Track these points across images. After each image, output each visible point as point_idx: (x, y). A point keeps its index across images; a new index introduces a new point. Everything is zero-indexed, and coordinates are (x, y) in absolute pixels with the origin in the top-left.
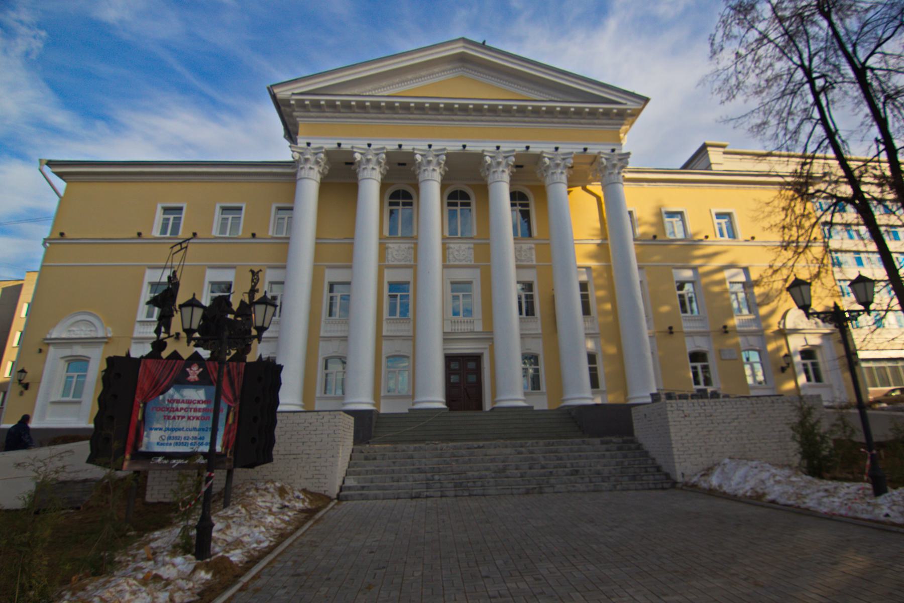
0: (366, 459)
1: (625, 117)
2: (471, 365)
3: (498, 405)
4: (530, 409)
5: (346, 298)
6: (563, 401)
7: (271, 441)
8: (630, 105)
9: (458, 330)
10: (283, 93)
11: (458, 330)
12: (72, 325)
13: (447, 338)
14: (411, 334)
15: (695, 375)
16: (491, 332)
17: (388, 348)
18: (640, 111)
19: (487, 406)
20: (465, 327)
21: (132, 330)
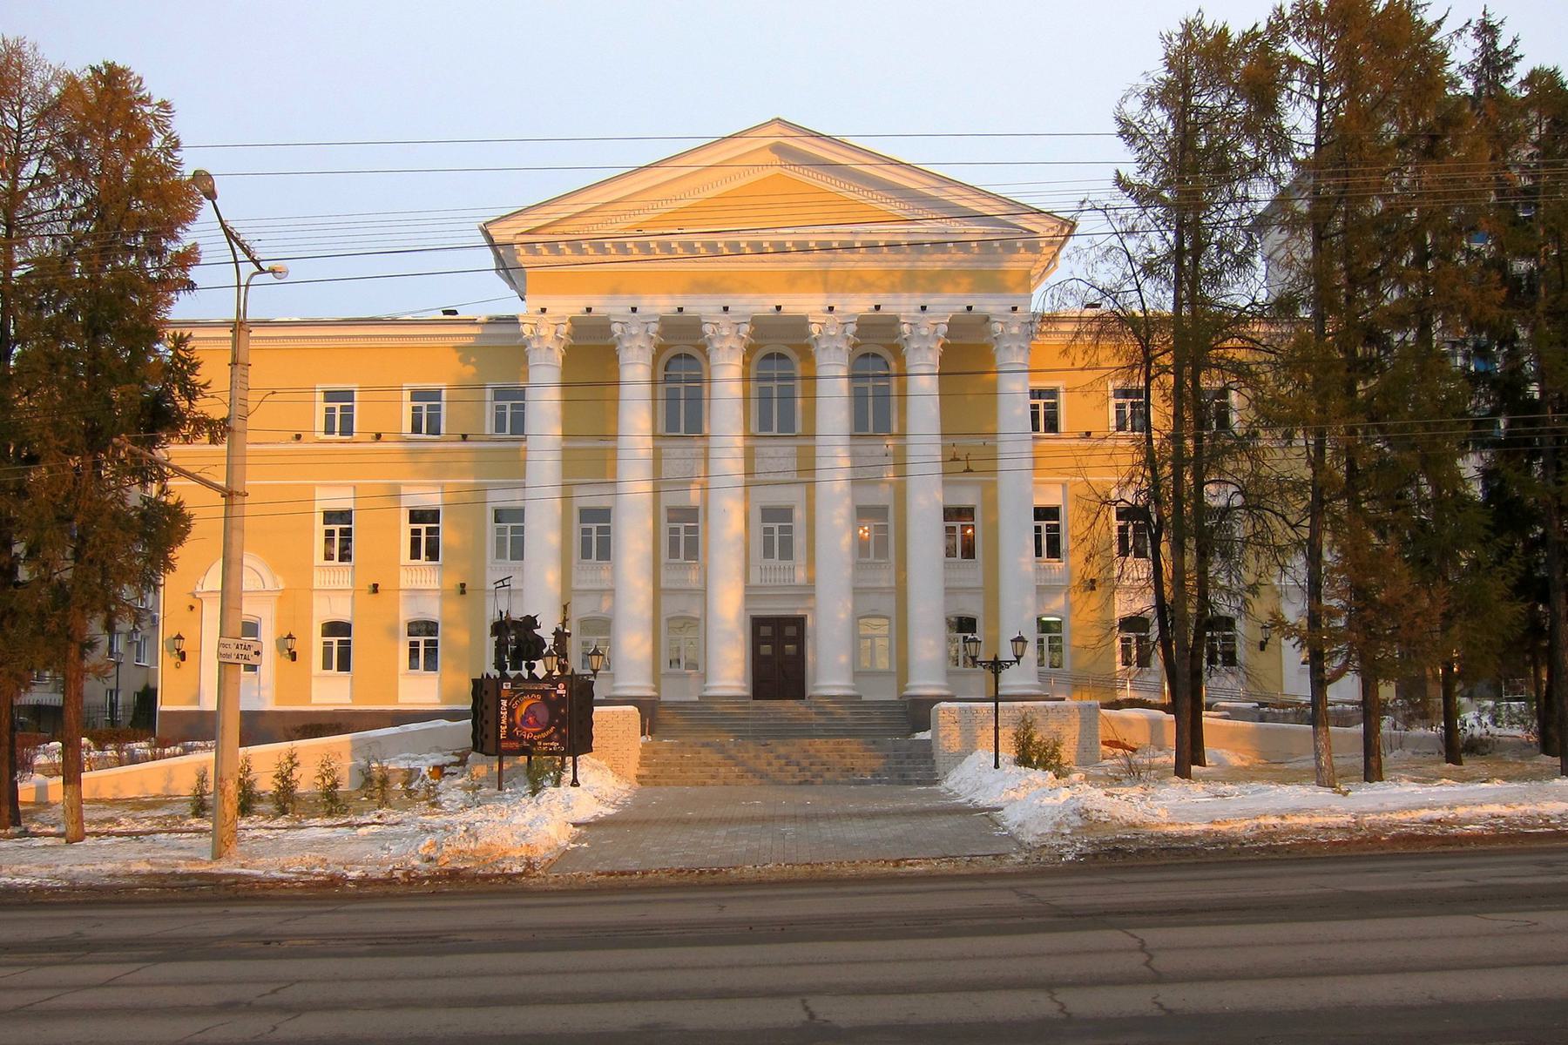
2: (791, 631)
5: (605, 532)
6: (615, 689)
9: (785, 580)
10: (501, 234)
11: (785, 580)
13: (750, 593)
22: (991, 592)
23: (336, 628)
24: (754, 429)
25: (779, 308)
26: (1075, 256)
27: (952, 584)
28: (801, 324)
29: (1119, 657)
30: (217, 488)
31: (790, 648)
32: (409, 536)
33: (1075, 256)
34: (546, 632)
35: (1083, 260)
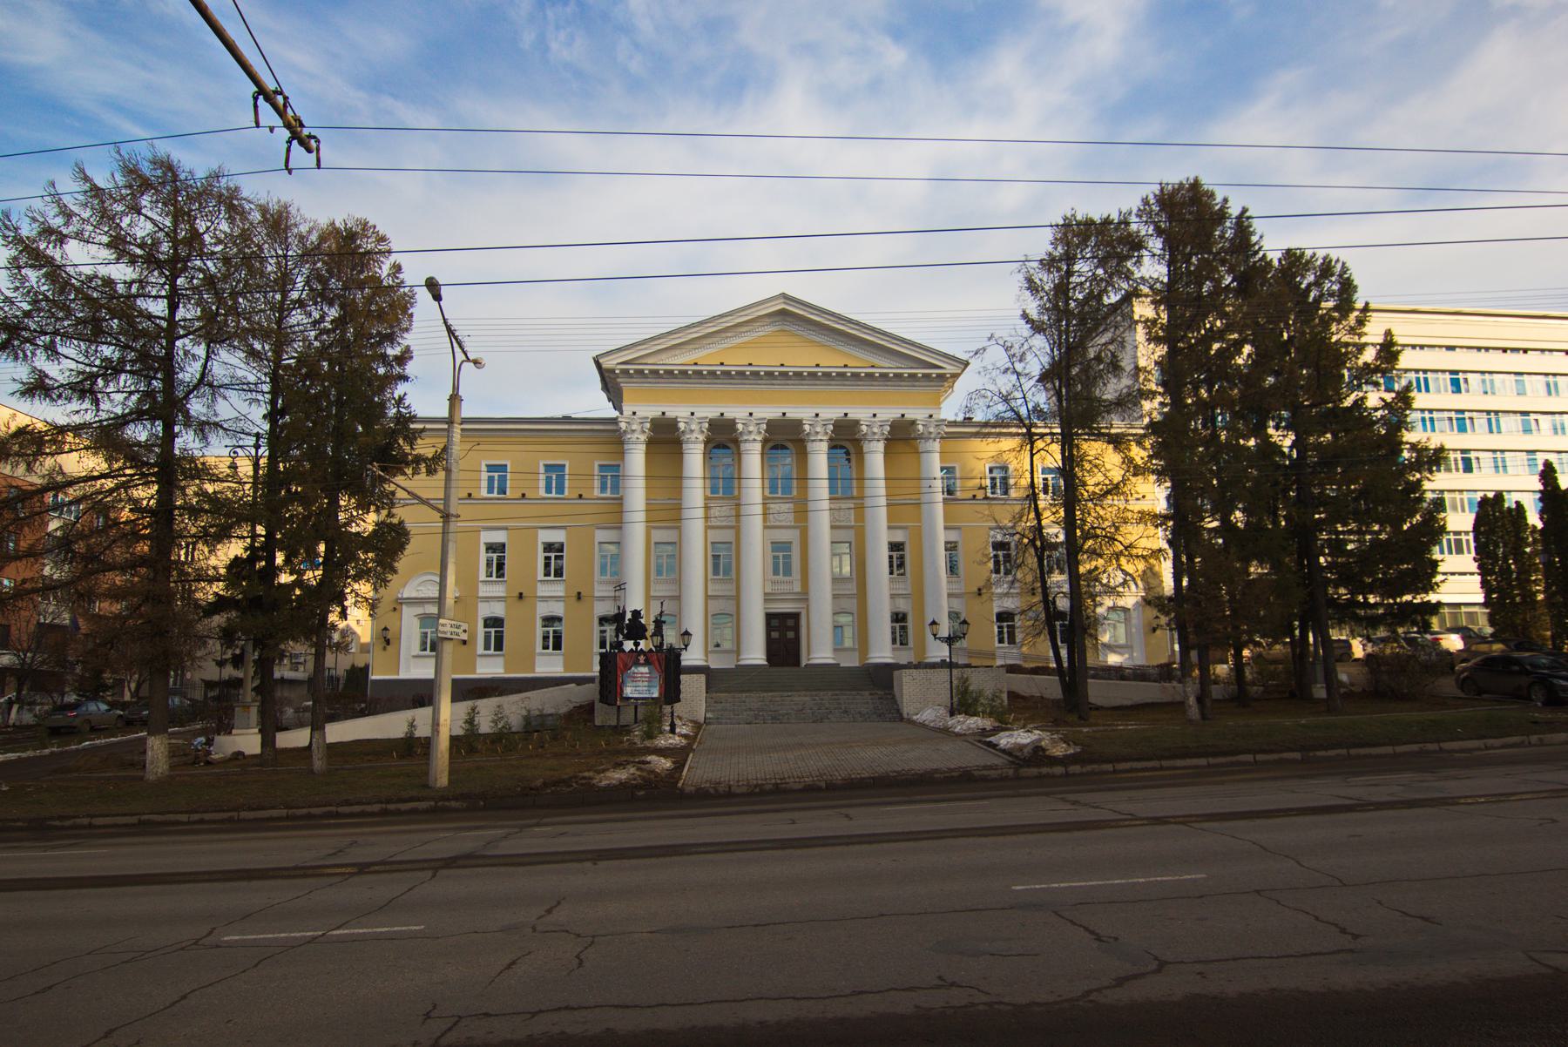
0: (716, 702)
1: (944, 381)
2: (790, 623)
3: (811, 662)
4: (837, 665)
7: (679, 691)
8: (950, 369)
10: (608, 363)
12: (419, 585)
13: (768, 598)
14: (734, 593)
15: (1001, 633)
16: (807, 594)
17: (715, 606)
18: (959, 375)
19: (804, 662)
20: (785, 588)
21: (477, 590)
22: (918, 596)
23: (494, 622)
24: (767, 493)
25: (784, 414)
26: (983, 374)
27: (894, 592)
28: (798, 424)
29: (996, 639)
30: (439, 510)
31: (791, 635)
32: (543, 561)
33: (983, 374)
34: (648, 621)
35: (988, 376)
